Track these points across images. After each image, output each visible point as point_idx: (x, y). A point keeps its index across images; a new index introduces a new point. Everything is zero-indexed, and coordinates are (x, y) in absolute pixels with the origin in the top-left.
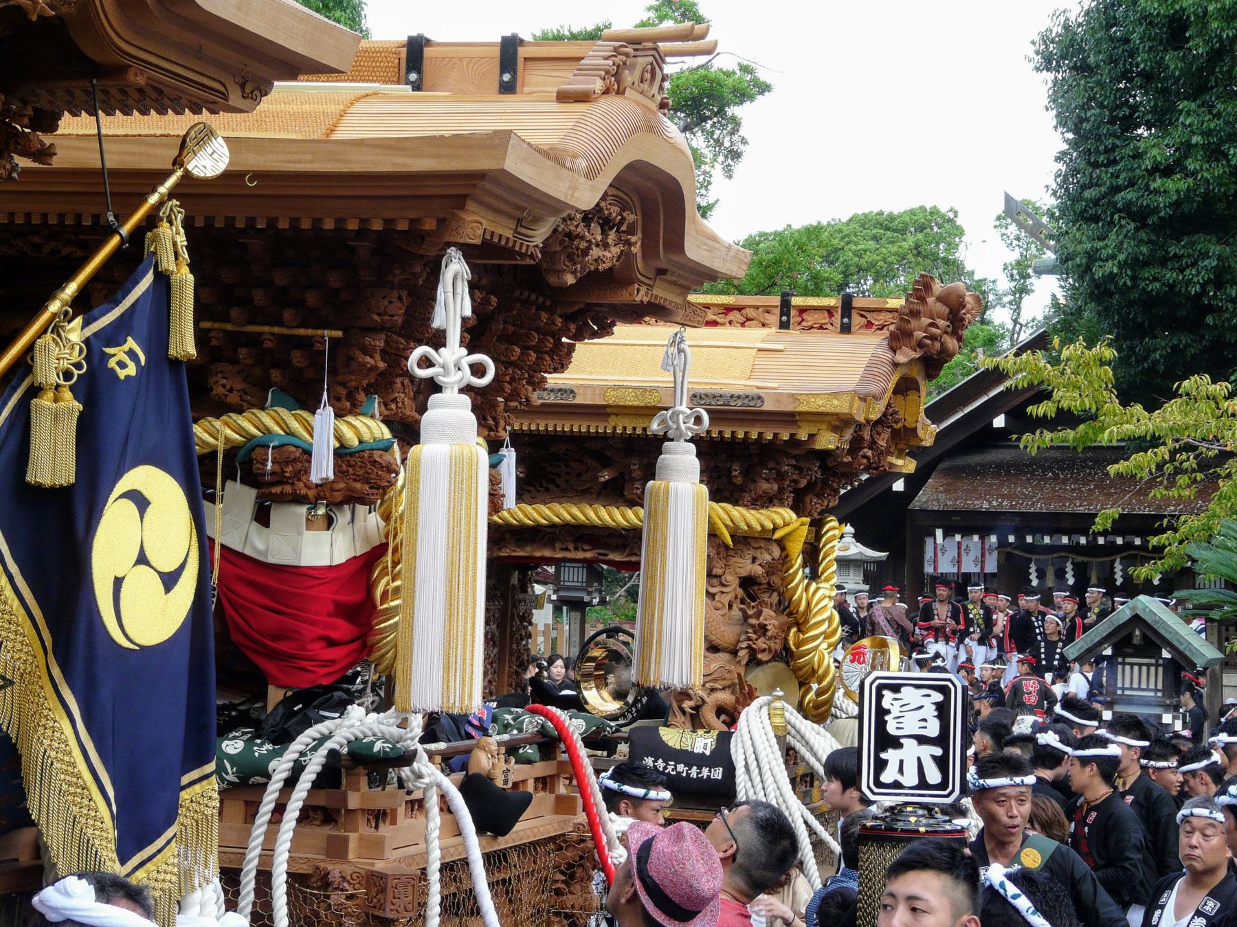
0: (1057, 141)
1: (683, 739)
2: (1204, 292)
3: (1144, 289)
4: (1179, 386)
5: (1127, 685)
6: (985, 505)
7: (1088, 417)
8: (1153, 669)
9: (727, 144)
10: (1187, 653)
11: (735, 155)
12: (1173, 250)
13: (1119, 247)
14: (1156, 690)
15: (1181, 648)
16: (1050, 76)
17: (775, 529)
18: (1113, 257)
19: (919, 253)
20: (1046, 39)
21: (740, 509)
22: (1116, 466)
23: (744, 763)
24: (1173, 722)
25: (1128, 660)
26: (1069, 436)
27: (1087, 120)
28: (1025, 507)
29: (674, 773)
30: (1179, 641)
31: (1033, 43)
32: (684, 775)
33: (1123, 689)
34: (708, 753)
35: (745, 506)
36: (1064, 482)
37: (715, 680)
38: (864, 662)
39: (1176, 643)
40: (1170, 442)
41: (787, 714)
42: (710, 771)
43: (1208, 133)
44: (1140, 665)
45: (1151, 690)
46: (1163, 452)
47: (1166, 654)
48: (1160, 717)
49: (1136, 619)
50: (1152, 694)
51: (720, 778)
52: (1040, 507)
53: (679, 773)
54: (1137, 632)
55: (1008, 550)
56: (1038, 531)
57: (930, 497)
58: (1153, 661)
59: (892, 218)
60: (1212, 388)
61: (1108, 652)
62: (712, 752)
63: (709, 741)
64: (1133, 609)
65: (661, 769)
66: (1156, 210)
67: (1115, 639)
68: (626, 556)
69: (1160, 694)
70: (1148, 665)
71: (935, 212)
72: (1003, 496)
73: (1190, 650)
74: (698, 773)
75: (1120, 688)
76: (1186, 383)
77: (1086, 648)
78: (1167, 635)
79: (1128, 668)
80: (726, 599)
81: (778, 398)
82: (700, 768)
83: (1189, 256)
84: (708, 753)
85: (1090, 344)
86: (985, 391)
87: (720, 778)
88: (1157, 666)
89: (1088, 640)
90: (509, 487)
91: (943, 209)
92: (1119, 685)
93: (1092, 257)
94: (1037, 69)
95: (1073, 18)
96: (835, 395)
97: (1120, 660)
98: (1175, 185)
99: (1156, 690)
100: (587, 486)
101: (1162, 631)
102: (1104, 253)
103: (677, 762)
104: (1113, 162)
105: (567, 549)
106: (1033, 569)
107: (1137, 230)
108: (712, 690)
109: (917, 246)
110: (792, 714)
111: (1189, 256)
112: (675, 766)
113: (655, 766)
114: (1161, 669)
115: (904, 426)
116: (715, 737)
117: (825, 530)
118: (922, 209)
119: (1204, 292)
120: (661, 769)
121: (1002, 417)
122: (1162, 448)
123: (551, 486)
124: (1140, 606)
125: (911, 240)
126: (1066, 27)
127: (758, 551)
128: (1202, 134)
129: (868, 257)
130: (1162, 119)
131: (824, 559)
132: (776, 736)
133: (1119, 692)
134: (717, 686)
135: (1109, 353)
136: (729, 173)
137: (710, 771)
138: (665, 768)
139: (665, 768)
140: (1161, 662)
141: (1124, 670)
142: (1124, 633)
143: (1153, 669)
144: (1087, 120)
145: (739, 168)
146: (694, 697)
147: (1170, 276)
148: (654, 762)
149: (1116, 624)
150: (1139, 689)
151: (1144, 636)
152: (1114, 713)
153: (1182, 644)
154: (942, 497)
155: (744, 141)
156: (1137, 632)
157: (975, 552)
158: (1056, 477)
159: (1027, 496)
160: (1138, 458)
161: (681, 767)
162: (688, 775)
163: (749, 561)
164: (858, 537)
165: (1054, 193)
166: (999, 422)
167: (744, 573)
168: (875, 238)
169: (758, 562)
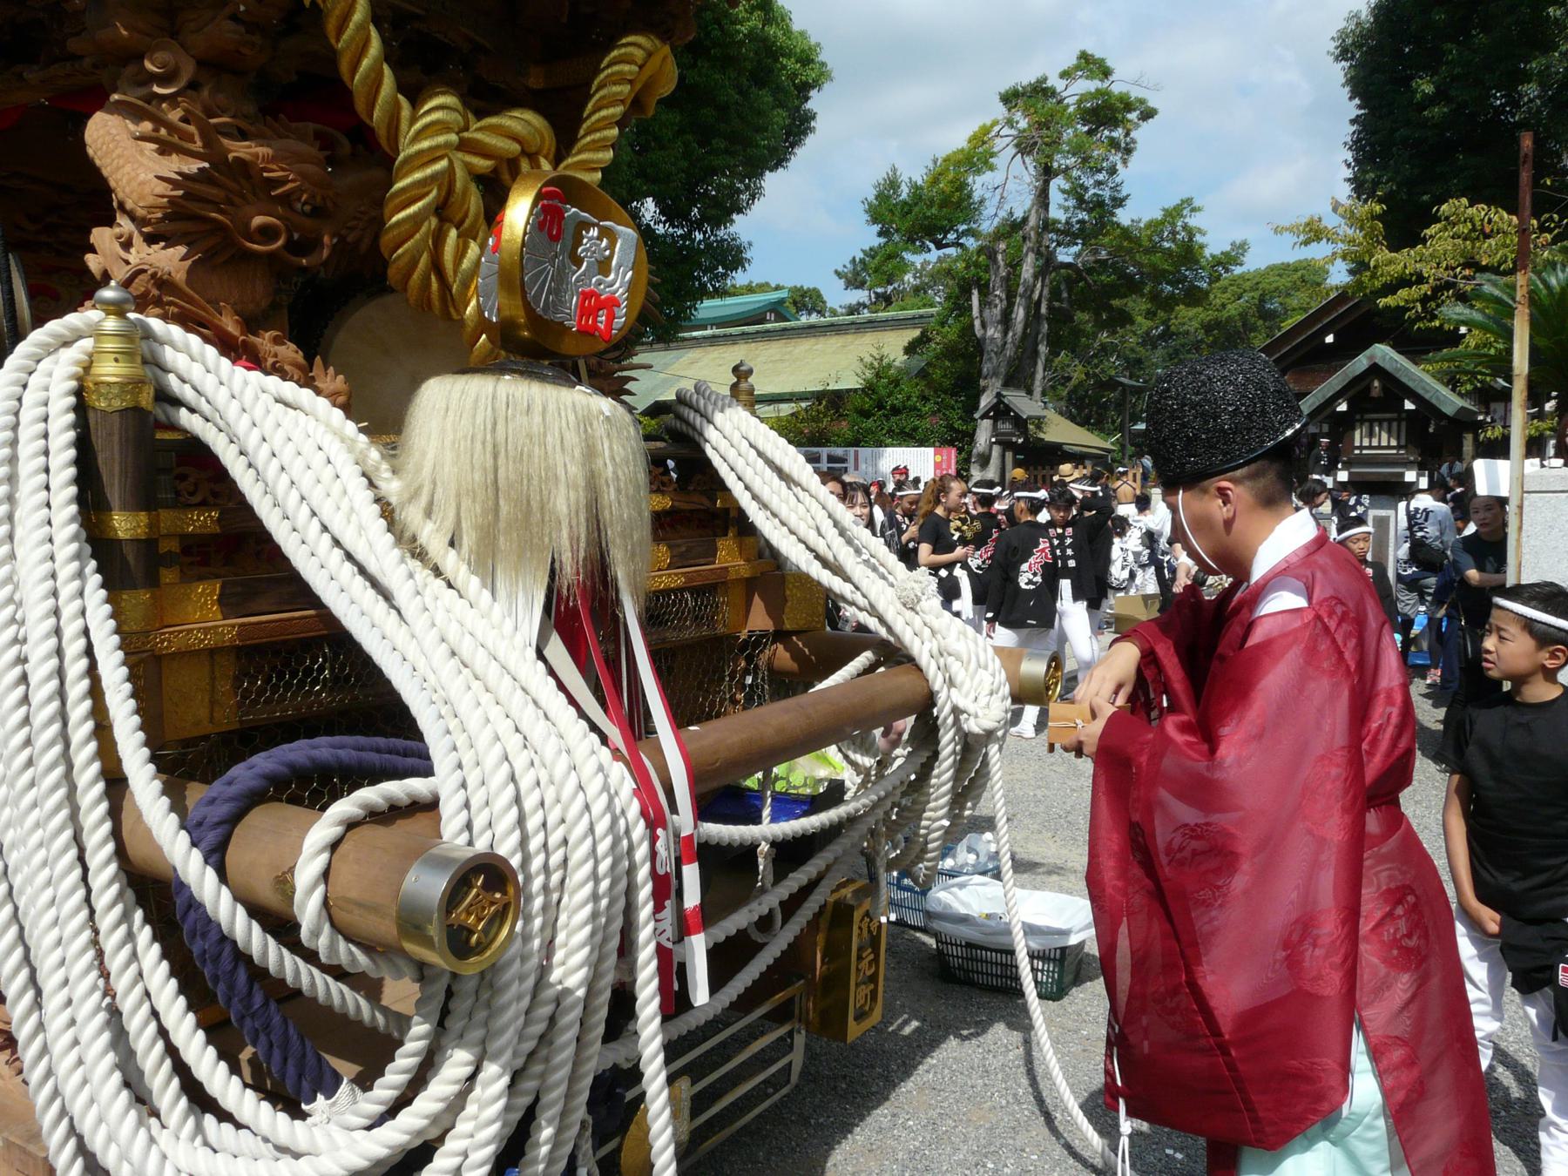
0: (1352, 109)
4: (1438, 210)
8: (1395, 425)
10: (1434, 401)
11: (1128, 151)
14: (1399, 447)
15: (1427, 396)
20: (1343, 35)
22: (1384, 300)
23: (830, 522)
25: (1367, 416)
30: (1424, 389)
31: (1333, 38)
39: (1421, 392)
40: (1431, 281)
45: (1393, 448)
46: (1425, 288)
47: (1409, 405)
48: (1403, 475)
49: (1375, 370)
54: (1376, 384)
58: (1395, 415)
59: (1288, 265)
60: (1471, 211)
61: (1343, 407)
64: (1371, 357)
67: (1351, 393)
70: (1393, 420)
73: (1438, 398)
75: (1357, 448)
76: (1444, 207)
78: (1410, 384)
86: (1320, 320)
88: (1399, 420)
89: (1320, 395)
90: (1392, 520)
92: (1357, 443)
94: (1337, 59)
97: (1358, 417)
99: (1399, 447)
101: (1404, 380)
109: (1303, 276)
114: (1404, 424)
117: (624, 41)
124: (1379, 354)
125: (1299, 274)
126: (1358, 24)
129: (1274, 285)
130: (1431, 67)
133: (1357, 452)
136: (1125, 162)
140: (1404, 415)
142: (1363, 384)
143: (1395, 425)
149: (1351, 376)
150: (1379, 447)
151: (1384, 388)
152: (1350, 474)
153: (1427, 392)
155: (1133, 141)
156: (1376, 384)
160: (1403, 293)
165: (1350, 148)
166: (1330, 339)
168: (1280, 275)
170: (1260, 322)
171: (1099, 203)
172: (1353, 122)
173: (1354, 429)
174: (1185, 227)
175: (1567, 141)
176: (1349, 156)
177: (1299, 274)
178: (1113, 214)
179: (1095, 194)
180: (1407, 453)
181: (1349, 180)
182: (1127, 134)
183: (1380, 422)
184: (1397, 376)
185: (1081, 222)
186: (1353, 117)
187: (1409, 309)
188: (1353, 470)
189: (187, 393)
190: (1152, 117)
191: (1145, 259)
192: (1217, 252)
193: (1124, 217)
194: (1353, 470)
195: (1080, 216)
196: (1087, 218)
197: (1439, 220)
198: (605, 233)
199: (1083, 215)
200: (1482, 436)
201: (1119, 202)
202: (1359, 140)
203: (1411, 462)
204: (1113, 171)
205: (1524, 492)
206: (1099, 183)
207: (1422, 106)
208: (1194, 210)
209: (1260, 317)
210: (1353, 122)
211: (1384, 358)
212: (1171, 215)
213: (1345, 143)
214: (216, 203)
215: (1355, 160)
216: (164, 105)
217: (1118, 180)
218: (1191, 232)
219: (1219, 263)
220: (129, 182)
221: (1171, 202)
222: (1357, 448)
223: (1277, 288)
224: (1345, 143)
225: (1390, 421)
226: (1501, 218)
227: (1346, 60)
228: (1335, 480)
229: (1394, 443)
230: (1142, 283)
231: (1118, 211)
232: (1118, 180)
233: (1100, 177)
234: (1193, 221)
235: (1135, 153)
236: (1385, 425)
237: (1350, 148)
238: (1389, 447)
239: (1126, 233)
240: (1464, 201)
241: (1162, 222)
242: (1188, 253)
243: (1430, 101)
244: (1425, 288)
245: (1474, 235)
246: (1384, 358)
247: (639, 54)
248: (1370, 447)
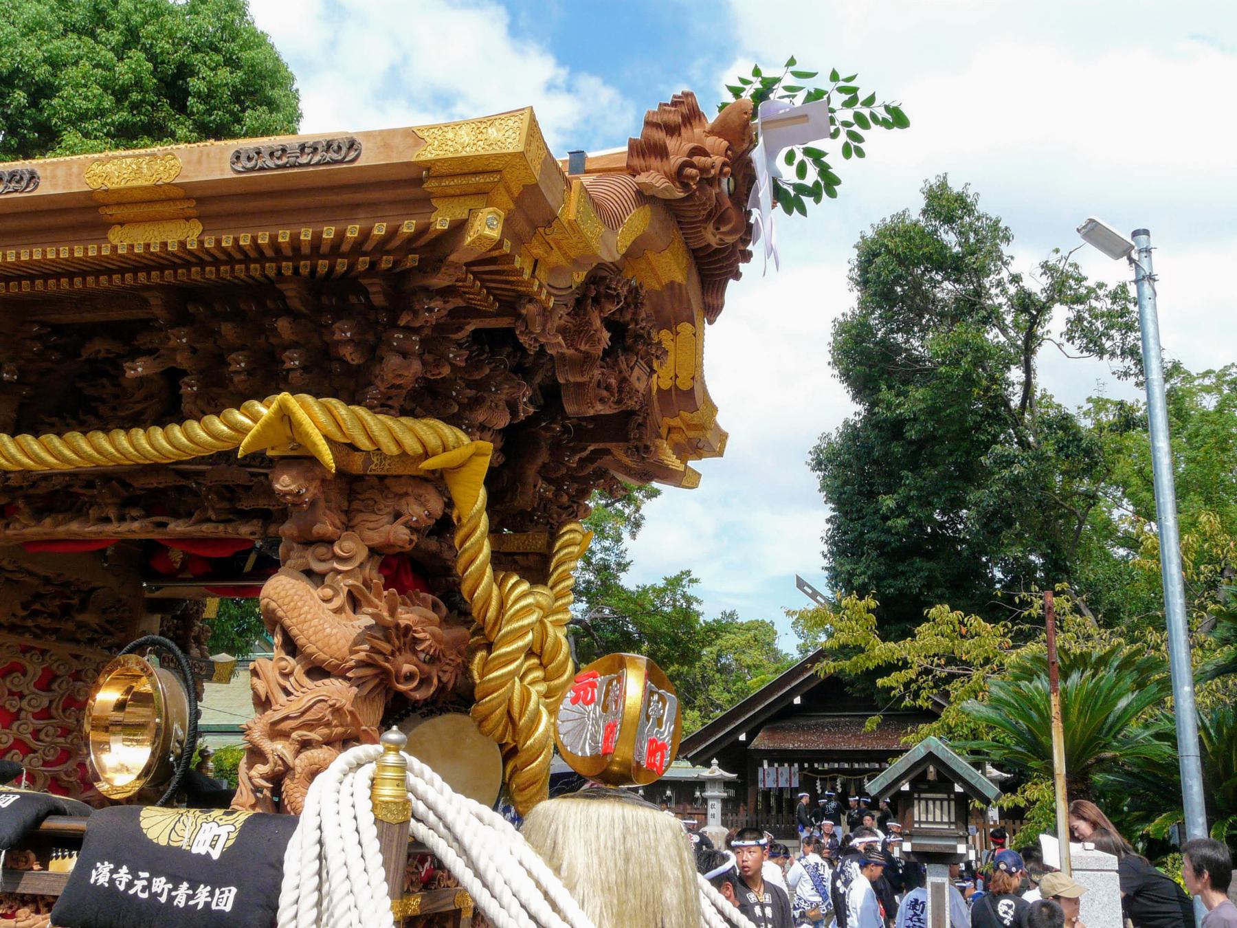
1: (179, 826)
2: (921, 593)
3: (884, 593)
4: (928, 613)
5: (923, 818)
6: (791, 746)
7: (859, 650)
8: (945, 803)
9: (633, 519)
10: (978, 787)
11: (637, 525)
12: (900, 568)
13: (868, 567)
14: (950, 823)
15: (973, 782)
16: (821, 474)
17: (426, 455)
18: (864, 573)
19: (756, 640)
20: (818, 450)
21: (361, 411)
24: (967, 852)
25: (923, 795)
26: (846, 664)
27: (845, 493)
28: (813, 747)
29: (145, 895)
31: (810, 452)
32: (163, 899)
33: (920, 822)
34: (216, 855)
35: (371, 408)
36: (835, 733)
37: (310, 726)
38: (592, 700)
39: (968, 778)
41: (412, 779)
42: (212, 894)
43: (921, 489)
44: (934, 800)
45: (945, 823)
47: (958, 789)
48: (955, 847)
49: (930, 757)
50: (947, 827)
51: (228, 909)
52: (821, 747)
53: (155, 896)
54: (931, 769)
55: (805, 772)
56: (821, 761)
57: (761, 742)
58: (945, 796)
61: (906, 787)
62: (223, 854)
63: (223, 831)
64: (927, 747)
65: (122, 888)
66: (889, 543)
67: (911, 776)
68: (194, 524)
69: (953, 827)
70: (941, 800)
71: (763, 622)
72: (801, 741)
73: (981, 784)
74: (190, 897)
75: (917, 822)
76: (933, 610)
77: (886, 784)
78: (958, 771)
79: (923, 803)
80: (344, 584)
81: (386, 138)
82: (194, 886)
83: (911, 571)
84: (216, 855)
85: (861, 598)
87: (228, 909)
88: (949, 800)
91: (768, 621)
92: (916, 819)
93: (851, 574)
94: (813, 469)
95: (833, 438)
96: (490, 120)
97: (916, 796)
98: (900, 522)
99: (950, 823)
100: (138, 407)
102: (858, 571)
103: (155, 873)
104: (862, 518)
105: (107, 520)
106: (818, 783)
107: (878, 556)
108: (305, 745)
109: (755, 636)
110: (430, 783)
111: (911, 571)
112: (150, 880)
113: (112, 881)
114: (953, 803)
115: (676, 387)
116: (238, 825)
118: (757, 621)
119: (921, 593)
120: (122, 888)
121: (799, 698)
122: (910, 671)
123: (91, 419)
124: (933, 745)
125: (752, 633)
127: (403, 502)
128: (917, 490)
129: (731, 642)
131: (556, 568)
132: (377, 821)
133: (916, 826)
134: (314, 735)
135: (873, 604)
136: (633, 535)
137: (212, 894)
138: (130, 885)
139: (130, 885)
141: (927, 805)
142: (920, 770)
144: (845, 493)
145: (641, 533)
146: (270, 757)
147: (900, 583)
148: (112, 872)
150: (934, 822)
151: (938, 773)
153: (973, 778)
154: (766, 742)
155: (642, 517)
156: (931, 769)
157: (786, 775)
158: (830, 730)
159: (814, 741)
161: (160, 884)
162: (171, 899)
163: (386, 519)
164: (721, 766)
165: (826, 542)
166: (797, 700)
167: (376, 538)
169: (403, 519)
170: (717, 676)
171: (603, 568)
172: (828, 521)
173: (913, 806)
174: (684, 596)
175: (5, 14)
176: (825, 548)
177: (752, 633)
178: (616, 577)
179: (601, 559)
180: (957, 828)
181: (826, 569)
182: (637, 510)
183: (934, 800)
184: (948, 763)
185: (589, 582)
186: (828, 517)
187: (894, 689)
188: (914, 842)
189: (421, 807)
190: (655, 496)
191: (647, 620)
192: (709, 620)
193: (629, 581)
194: (914, 842)
195: (587, 577)
196: (593, 578)
197: (928, 621)
198: (661, 698)
199: (590, 576)
200: (971, 806)
201: (623, 567)
202: (833, 537)
203: (961, 837)
204: (618, 540)
205: (1072, 870)
206: (606, 549)
207: (885, 518)
208: (691, 581)
209: (718, 671)
210: (828, 521)
211: (937, 747)
212: (672, 585)
213: (822, 538)
214: (384, 655)
215: (830, 552)
216: (339, 577)
217: (622, 547)
218: (689, 600)
219: (712, 630)
220: (315, 633)
221: (674, 573)
222: (917, 822)
223: (733, 646)
224: (822, 538)
225: (941, 800)
226: (979, 624)
227: (820, 470)
228: (901, 850)
229: (946, 819)
230: (641, 642)
231: (622, 575)
232: (622, 547)
233: (607, 543)
234: (690, 591)
235: (642, 528)
236: (938, 803)
237: (826, 542)
238: (942, 823)
239: (628, 597)
240: (947, 607)
241: (664, 590)
242: (686, 617)
243: (893, 514)
244: (911, 674)
245: (954, 635)
246: (937, 747)
247: (579, 537)
248: (927, 822)
